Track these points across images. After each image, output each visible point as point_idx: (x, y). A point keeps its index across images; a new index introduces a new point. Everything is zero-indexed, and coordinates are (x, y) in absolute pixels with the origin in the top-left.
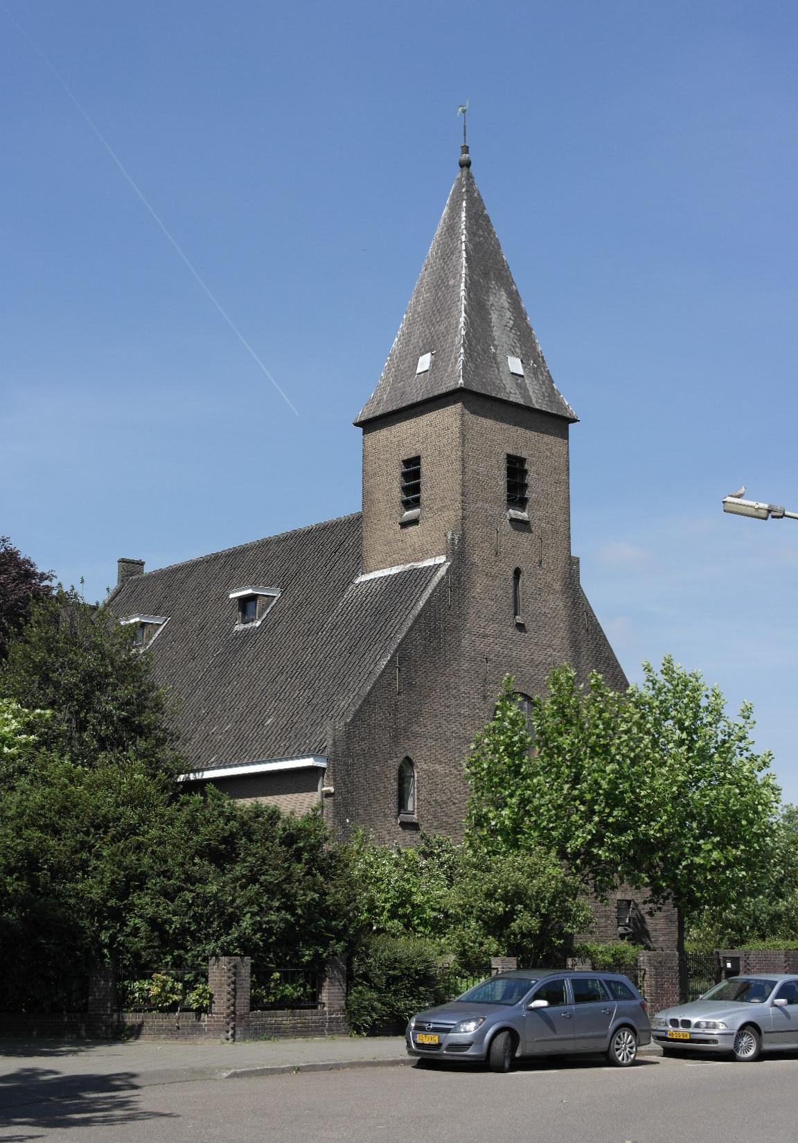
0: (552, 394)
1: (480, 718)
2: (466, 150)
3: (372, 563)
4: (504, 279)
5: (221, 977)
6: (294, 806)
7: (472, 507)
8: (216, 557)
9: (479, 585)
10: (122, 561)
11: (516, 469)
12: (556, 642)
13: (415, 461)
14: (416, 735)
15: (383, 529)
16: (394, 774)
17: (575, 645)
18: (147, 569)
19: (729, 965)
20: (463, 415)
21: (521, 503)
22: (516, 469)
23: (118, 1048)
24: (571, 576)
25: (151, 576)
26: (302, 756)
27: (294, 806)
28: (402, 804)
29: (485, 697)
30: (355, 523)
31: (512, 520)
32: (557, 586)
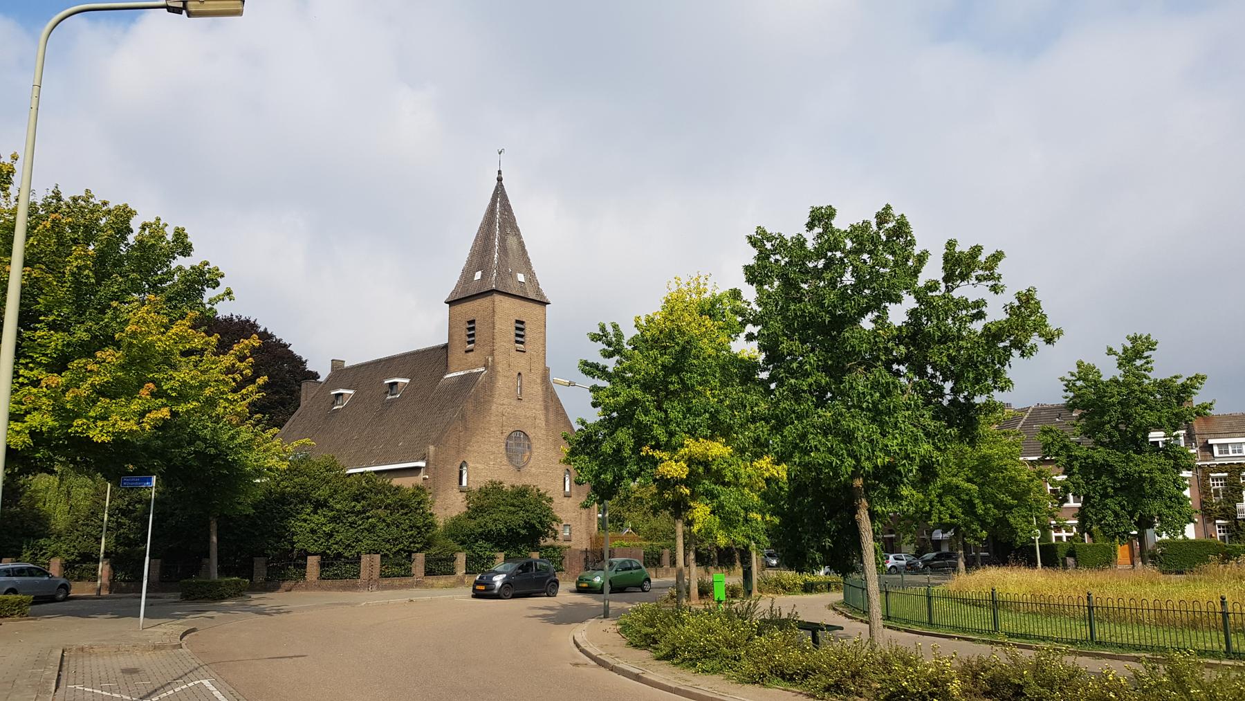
0: (538, 291)
3: (451, 369)
5: (370, 564)
6: (407, 482)
8: (380, 361)
9: (500, 383)
11: (520, 325)
13: (472, 322)
15: (456, 355)
16: (457, 470)
18: (346, 365)
23: (349, 593)
25: (348, 369)
27: (407, 482)
28: (461, 483)
30: (446, 347)
32: (539, 381)
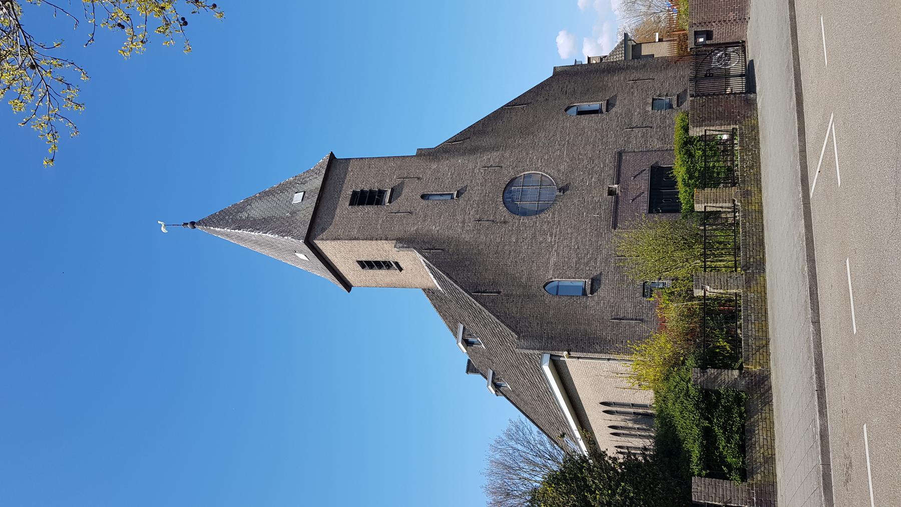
0: (315, 172)
1: (519, 226)
2: (186, 224)
4: (240, 208)
7: (380, 232)
10: (467, 372)
11: (362, 198)
12: (470, 166)
14: (529, 279)
17: (473, 151)
19: (701, 40)
20: (322, 239)
21: (381, 193)
22: (362, 198)
24: (429, 154)
26: (542, 375)
29: (505, 222)
31: (390, 202)
